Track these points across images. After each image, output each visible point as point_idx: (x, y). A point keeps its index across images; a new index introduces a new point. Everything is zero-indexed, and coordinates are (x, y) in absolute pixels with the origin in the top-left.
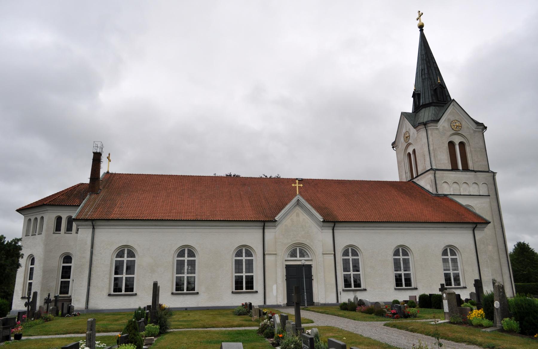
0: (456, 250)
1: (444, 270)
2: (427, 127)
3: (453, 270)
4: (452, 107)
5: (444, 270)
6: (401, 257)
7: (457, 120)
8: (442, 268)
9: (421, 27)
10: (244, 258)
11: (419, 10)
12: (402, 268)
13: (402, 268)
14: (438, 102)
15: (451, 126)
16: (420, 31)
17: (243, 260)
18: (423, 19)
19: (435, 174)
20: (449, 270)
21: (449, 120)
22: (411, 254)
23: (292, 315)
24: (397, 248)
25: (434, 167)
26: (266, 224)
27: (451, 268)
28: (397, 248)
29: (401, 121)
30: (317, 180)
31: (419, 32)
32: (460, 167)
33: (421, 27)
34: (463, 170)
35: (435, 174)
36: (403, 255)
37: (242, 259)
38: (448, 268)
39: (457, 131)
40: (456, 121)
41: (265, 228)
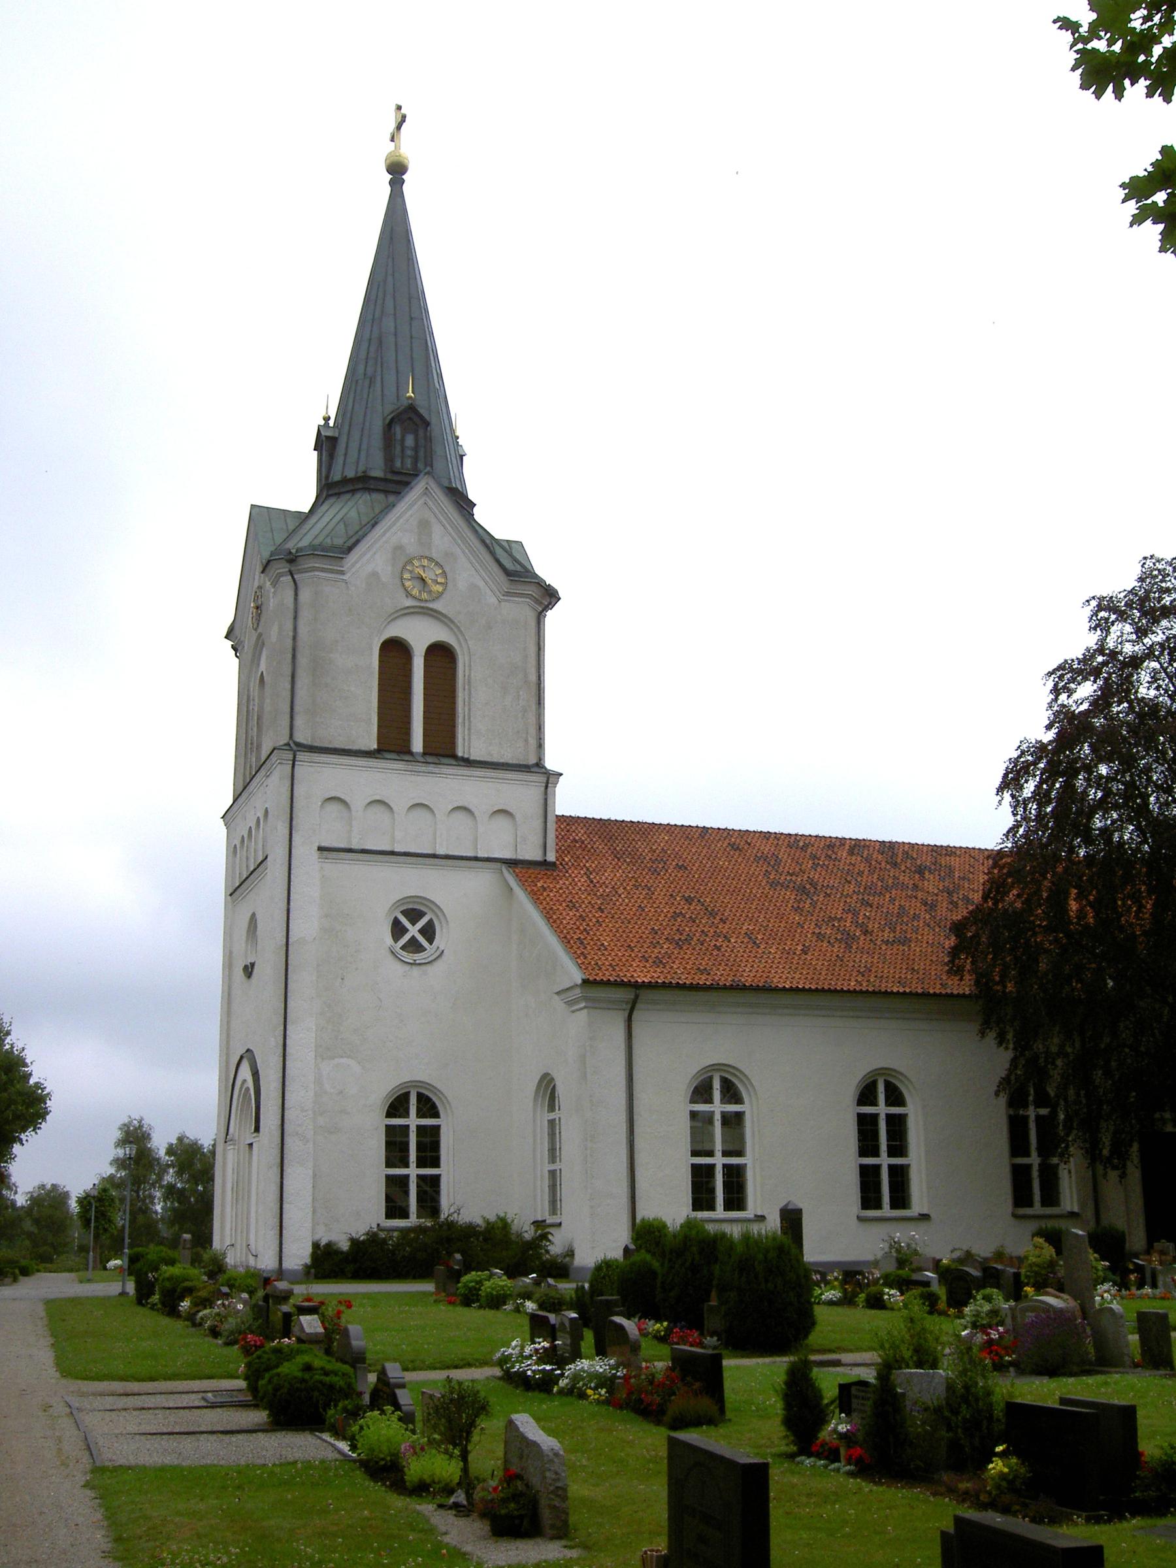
0: (735, 1076)
1: (695, 1153)
2: (300, 572)
3: (726, 1154)
4: (421, 502)
5: (695, 1153)
6: (717, 1107)
7: (430, 559)
8: (685, 1146)
9: (397, 170)
10: (413, 1121)
11: (399, 104)
12: (884, 1147)
13: (884, 1147)
14: (389, 476)
15: (402, 578)
16: (391, 183)
17: (408, 1126)
18: (409, 149)
19: (546, 787)
20: (710, 1154)
21: (399, 548)
22: (750, 1096)
23: (560, 1331)
24: (706, 1073)
25: (300, 737)
26: (645, 995)
27: (718, 1147)
28: (706, 1073)
29: (250, 541)
30: (567, 817)
31: (387, 190)
32: (417, 745)
33: (397, 170)
34: (425, 754)
35: (546, 787)
36: (889, 1103)
37: (407, 1123)
38: (707, 1147)
39: (426, 601)
40: (425, 562)
41: (638, 1006)
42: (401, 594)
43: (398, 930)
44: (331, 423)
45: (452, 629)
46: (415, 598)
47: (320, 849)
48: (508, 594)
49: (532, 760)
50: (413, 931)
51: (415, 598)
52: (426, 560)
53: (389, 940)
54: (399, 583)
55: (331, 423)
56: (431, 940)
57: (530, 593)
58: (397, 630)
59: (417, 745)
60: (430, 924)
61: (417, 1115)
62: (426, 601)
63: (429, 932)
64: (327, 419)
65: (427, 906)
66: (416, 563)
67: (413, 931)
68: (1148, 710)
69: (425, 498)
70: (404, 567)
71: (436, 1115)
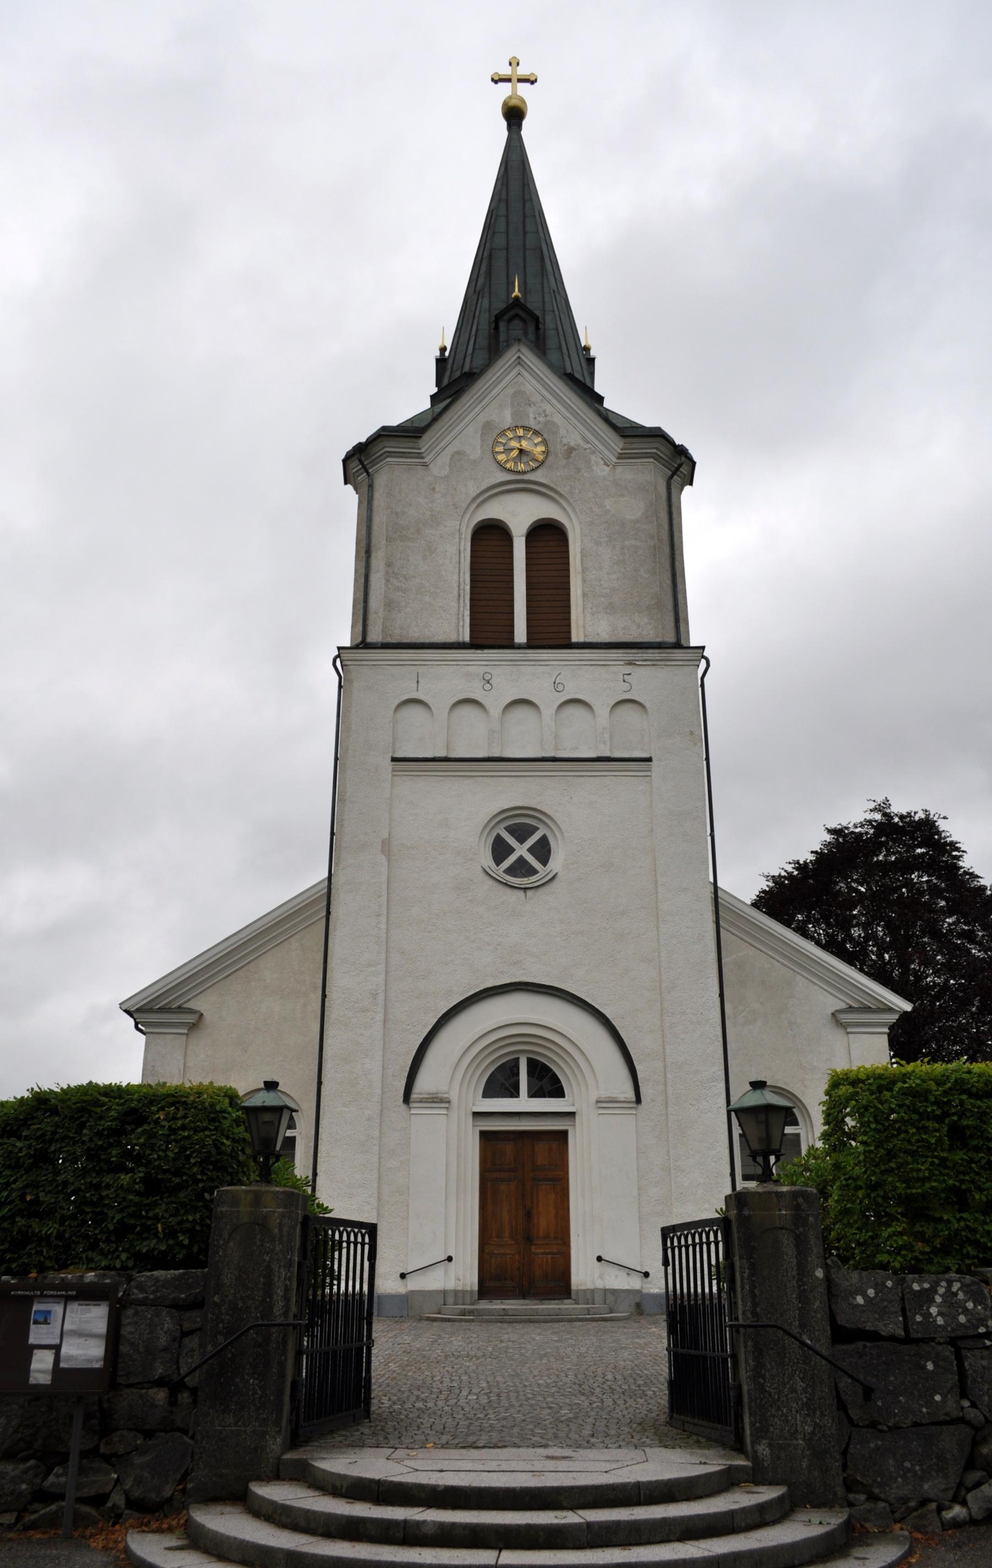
7: (527, 429)
32: (520, 634)
40: (520, 432)
42: (494, 467)
43: (500, 850)
44: (447, 354)
45: (564, 509)
46: (510, 471)
47: (394, 760)
48: (621, 456)
49: (670, 638)
50: (522, 851)
51: (510, 471)
52: (521, 430)
53: (488, 861)
54: (492, 457)
55: (447, 354)
56: (544, 860)
57: (655, 451)
58: (495, 510)
59: (520, 634)
60: (544, 842)
61: (516, 1097)
62: (524, 473)
63: (543, 851)
64: (443, 350)
65: (540, 820)
66: (510, 434)
67: (522, 851)
68: (943, 955)
69: (519, 368)
70: (496, 442)
71: (558, 1092)
